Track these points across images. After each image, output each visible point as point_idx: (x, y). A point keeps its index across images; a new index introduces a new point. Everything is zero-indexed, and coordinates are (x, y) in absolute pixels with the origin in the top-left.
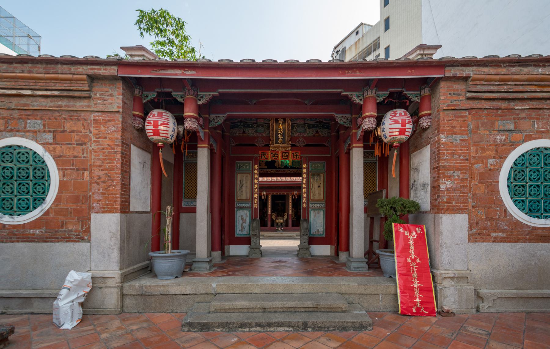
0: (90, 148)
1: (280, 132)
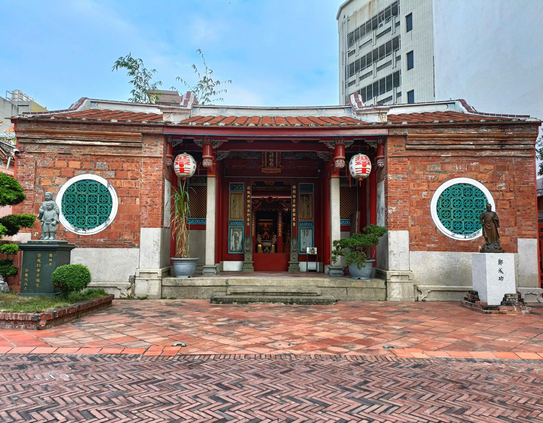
0: (140, 182)
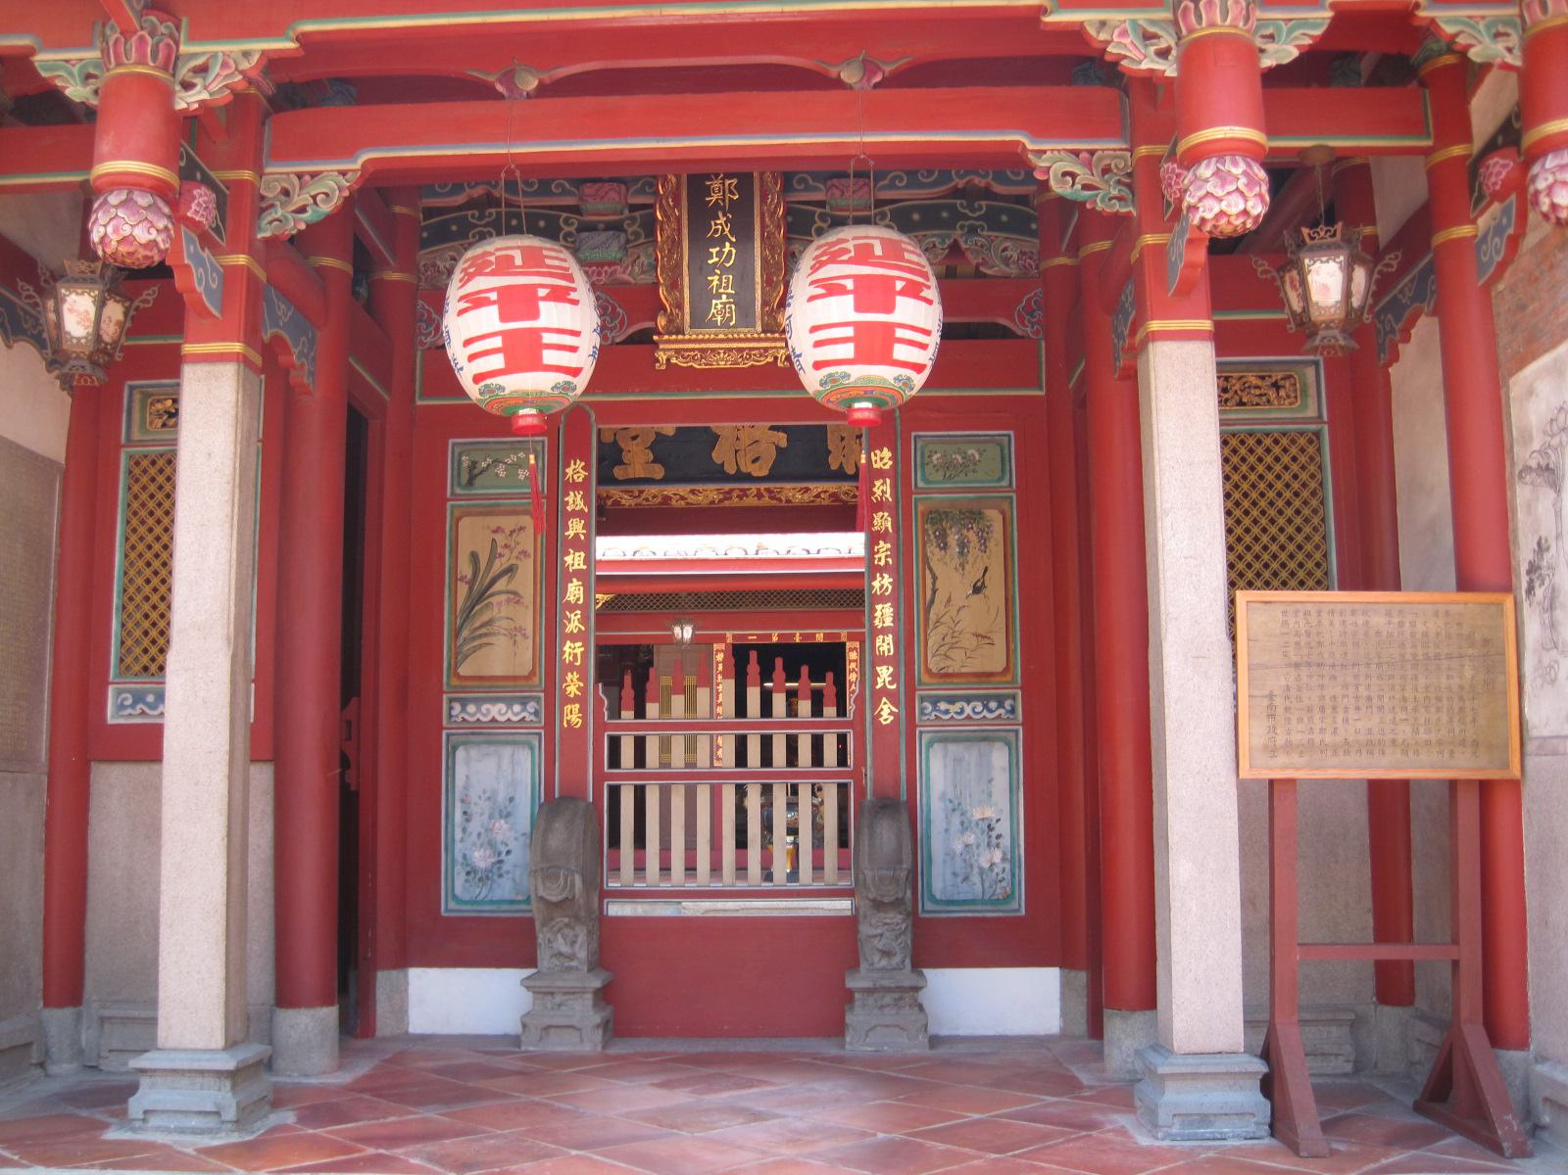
1: (720, 254)
